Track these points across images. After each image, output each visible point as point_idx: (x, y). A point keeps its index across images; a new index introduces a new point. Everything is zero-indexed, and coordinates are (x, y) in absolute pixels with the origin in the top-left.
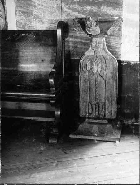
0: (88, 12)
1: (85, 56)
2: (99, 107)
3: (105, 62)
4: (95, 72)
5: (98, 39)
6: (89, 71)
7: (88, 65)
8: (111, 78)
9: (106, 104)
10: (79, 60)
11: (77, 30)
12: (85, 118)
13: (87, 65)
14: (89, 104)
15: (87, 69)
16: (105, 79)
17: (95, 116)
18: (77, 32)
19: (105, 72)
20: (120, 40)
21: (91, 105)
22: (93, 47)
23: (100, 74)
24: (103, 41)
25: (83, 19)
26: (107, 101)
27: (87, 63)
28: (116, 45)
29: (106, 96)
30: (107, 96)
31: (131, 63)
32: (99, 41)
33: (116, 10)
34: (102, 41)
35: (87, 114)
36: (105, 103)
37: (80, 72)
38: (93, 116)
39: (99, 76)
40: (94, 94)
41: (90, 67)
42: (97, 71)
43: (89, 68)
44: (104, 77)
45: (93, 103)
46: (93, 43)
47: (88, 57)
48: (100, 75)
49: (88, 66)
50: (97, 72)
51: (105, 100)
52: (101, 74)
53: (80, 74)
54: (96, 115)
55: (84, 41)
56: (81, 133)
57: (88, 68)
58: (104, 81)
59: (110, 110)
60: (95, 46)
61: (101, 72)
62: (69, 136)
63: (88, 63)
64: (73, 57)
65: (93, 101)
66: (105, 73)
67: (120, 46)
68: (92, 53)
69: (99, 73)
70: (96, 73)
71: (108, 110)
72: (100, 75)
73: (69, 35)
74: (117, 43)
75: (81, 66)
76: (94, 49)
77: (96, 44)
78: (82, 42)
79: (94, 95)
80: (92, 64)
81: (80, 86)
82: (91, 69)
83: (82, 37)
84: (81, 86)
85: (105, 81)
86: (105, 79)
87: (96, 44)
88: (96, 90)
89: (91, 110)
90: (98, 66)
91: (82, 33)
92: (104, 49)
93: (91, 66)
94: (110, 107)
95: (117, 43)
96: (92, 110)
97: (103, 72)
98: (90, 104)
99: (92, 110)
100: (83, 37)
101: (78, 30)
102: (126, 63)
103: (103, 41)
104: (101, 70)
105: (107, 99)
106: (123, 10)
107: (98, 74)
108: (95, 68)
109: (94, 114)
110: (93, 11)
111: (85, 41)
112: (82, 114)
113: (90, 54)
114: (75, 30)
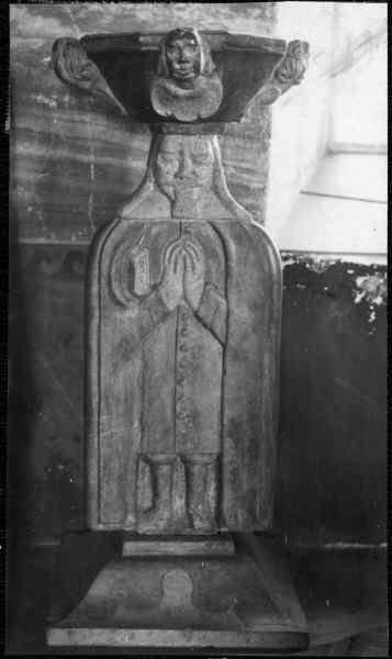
0: (109, 17)
1: (125, 224)
2: (188, 474)
3: (220, 252)
4: (171, 305)
5: (190, 145)
6: (142, 299)
7: (137, 266)
8: (250, 330)
9: (226, 460)
10: (92, 249)
11: (54, 104)
12: (116, 539)
13: (131, 270)
14: (137, 463)
15: (131, 287)
16: (223, 339)
17: (169, 520)
18: (56, 115)
19: (223, 301)
20: (262, 156)
21: (147, 469)
22: (163, 181)
23: (196, 315)
24: (214, 150)
25: (141, 39)
26: (228, 443)
27: (137, 260)
28: (245, 176)
29: (226, 422)
30: (232, 421)
31: (311, 262)
32: (194, 153)
33: (247, 16)
34: (210, 150)
35: (131, 518)
36: (220, 457)
37: (95, 303)
38: (162, 524)
39: (191, 324)
40: (169, 412)
41: (146, 277)
42: (185, 298)
43: (142, 283)
44: (219, 327)
45: (161, 457)
46: (165, 160)
47: (137, 228)
48: (199, 319)
49: (138, 271)
50: (183, 303)
51: (222, 443)
52: (201, 314)
53: (96, 313)
54: (172, 515)
55: (85, 158)
56: (101, 619)
57: (137, 281)
58: (216, 346)
59: (245, 487)
60: (176, 176)
61: (202, 302)
62: (44, 638)
63: (141, 258)
64: (31, 235)
65: (159, 449)
66: (223, 307)
67: (265, 182)
68: (161, 209)
69: (195, 305)
70: (179, 307)
71: (234, 490)
72: (199, 319)
73: (19, 129)
74: (248, 171)
75: (105, 272)
76: (170, 190)
77: (182, 166)
78: (74, 163)
79: (164, 420)
80: (155, 263)
81: (94, 375)
82: (155, 288)
83: (78, 138)
84: (103, 373)
85: (224, 346)
86: (223, 339)
87: (182, 166)
88: (179, 389)
89: (148, 492)
90: (189, 274)
91: (77, 117)
92: (216, 187)
93: (153, 275)
94: (244, 476)
95: (248, 171)
96: (156, 495)
97: (213, 304)
98: (142, 464)
99: (156, 495)
100: (85, 139)
101: (61, 105)
102: (291, 262)
103: (214, 150)
104: (205, 294)
105: (231, 436)
106: (279, 16)
107: (191, 313)
108: (174, 284)
109: (166, 514)
110: (134, 16)
111: (92, 158)
112: (103, 519)
113: (149, 216)
114: (45, 106)
